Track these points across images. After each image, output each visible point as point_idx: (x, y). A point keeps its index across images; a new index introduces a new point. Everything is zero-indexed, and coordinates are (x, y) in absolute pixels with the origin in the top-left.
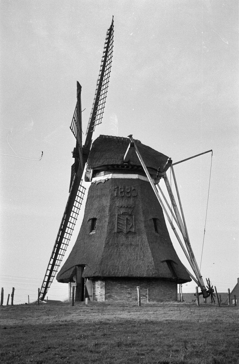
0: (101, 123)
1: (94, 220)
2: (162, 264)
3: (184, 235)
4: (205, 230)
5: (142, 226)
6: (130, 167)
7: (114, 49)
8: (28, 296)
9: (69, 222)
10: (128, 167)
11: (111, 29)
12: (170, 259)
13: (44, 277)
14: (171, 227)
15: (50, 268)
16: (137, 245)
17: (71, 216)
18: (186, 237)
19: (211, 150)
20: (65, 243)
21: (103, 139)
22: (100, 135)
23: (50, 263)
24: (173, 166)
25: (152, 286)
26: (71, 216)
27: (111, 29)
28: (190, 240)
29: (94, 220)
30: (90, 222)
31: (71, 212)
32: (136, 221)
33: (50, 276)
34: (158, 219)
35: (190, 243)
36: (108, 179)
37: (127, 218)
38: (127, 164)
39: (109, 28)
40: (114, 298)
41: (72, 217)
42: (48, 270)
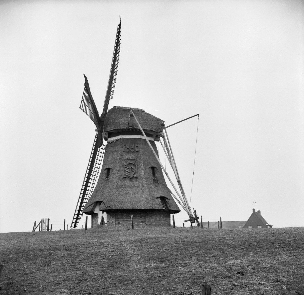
0: (113, 98)
1: (109, 169)
2: (156, 199)
3: (177, 178)
4: (193, 174)
5: (142, 173)
6: (134, 130)
7: (120, 49)
8: (68, 225)
9: (97, 155)
10: (132, 130)
11: (120, 25)
12: (163, 195)
13: (78, 198)
14: (165, 173)
15: (80, 201)
16: (139, 186)
17: (98, 151)
18: (178, 179)
19: (198, 115)
20: (91, 186)
21: (116, 110)
22: (114, 106)
23: (79, 201)
24: (166, 129)
25: (149, 215)
26: (98, 151)
27: (120, 25)
28: (181, 181)
29: (109, 169)
30: (106, 171)
31: (92, 172)
32: (138, 169)
33: (79, 211)
34: (155, 167)
35: (181, 184)
36: (118, 139)
37: (131, 167)
38: (131, 127)
39: (119, 24)
40: (122, 224)
41: (98, 156)
42: (83, 185)
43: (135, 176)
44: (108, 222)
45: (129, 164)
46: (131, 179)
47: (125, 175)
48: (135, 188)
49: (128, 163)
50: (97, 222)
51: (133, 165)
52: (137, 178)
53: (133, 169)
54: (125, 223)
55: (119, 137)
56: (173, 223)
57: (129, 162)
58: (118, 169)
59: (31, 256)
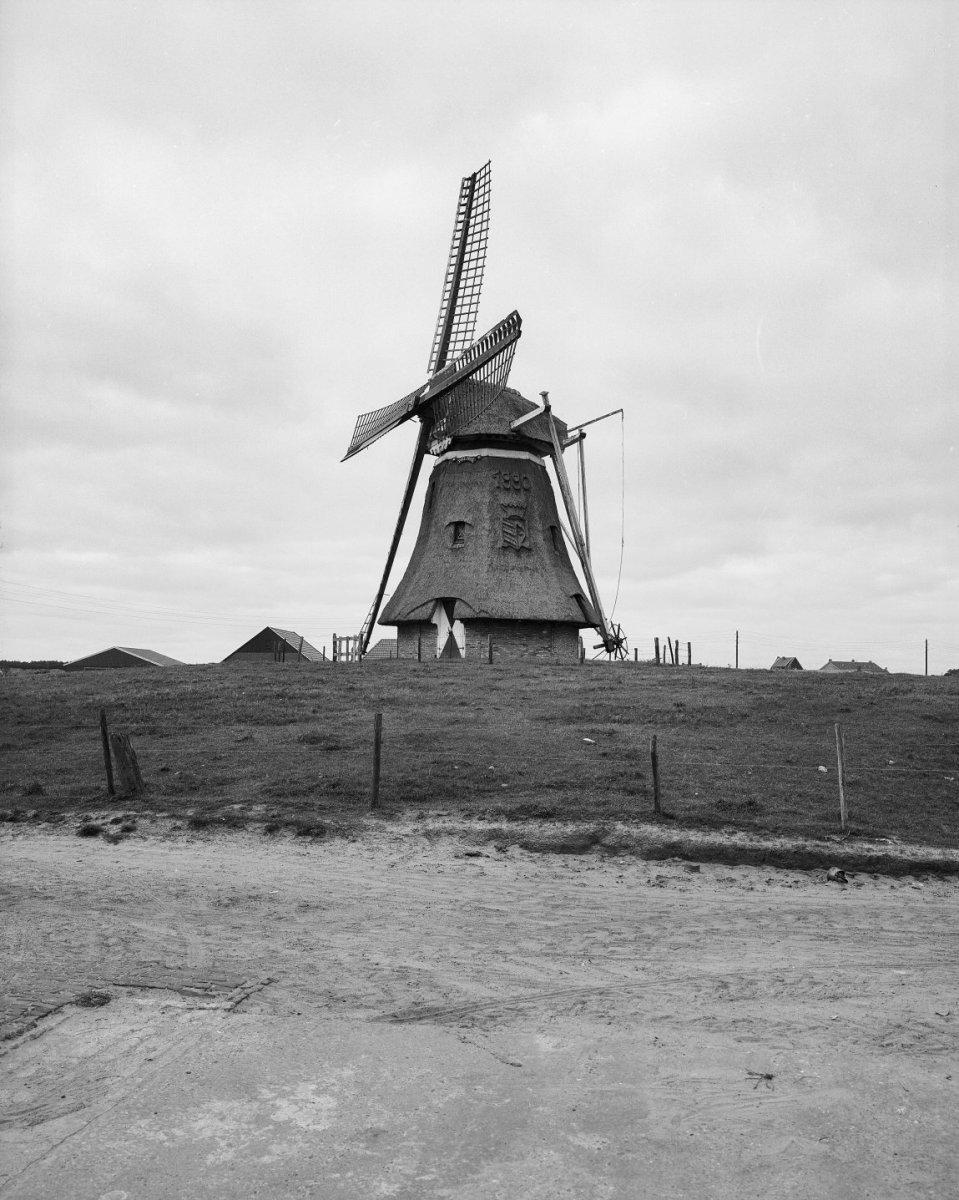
36: (482, 457)
43: (527, 545)
44: (467, 645)
45: (512, 518)
46: (519, 551)
47: (505, 541)
48: (529, 572)
49: (509, 514)
50: (434, 645)
51: (522, 520)
52: (530, 550)
53: (521, 528)
54: (508, 648)
55: (485, 452)
56: (480, 436)
57: (511, 512)
58: (487, 525)
59: (887, 764)
